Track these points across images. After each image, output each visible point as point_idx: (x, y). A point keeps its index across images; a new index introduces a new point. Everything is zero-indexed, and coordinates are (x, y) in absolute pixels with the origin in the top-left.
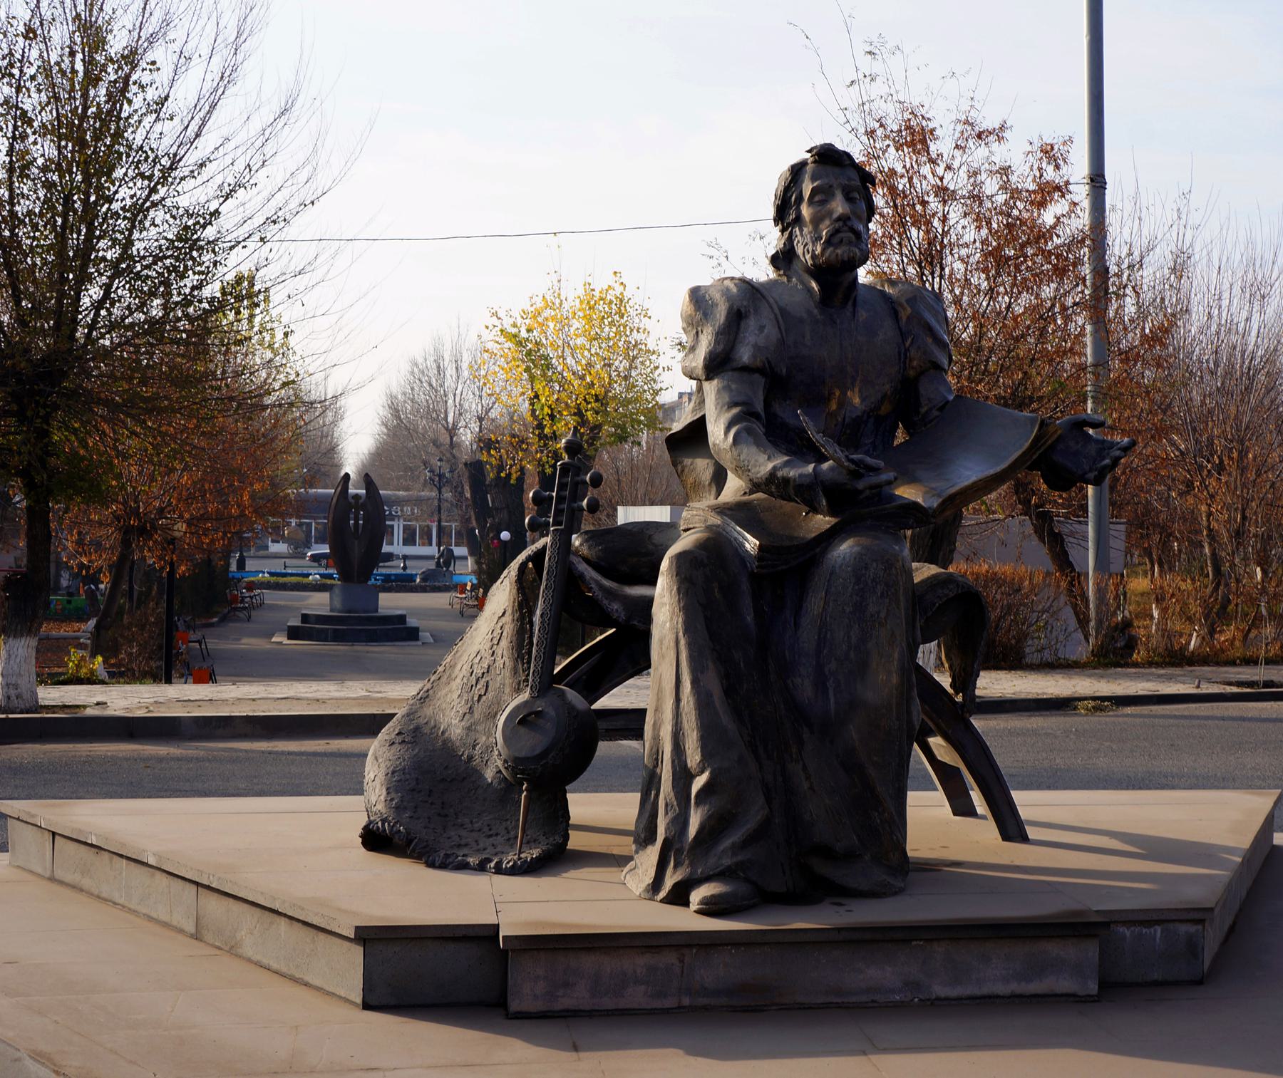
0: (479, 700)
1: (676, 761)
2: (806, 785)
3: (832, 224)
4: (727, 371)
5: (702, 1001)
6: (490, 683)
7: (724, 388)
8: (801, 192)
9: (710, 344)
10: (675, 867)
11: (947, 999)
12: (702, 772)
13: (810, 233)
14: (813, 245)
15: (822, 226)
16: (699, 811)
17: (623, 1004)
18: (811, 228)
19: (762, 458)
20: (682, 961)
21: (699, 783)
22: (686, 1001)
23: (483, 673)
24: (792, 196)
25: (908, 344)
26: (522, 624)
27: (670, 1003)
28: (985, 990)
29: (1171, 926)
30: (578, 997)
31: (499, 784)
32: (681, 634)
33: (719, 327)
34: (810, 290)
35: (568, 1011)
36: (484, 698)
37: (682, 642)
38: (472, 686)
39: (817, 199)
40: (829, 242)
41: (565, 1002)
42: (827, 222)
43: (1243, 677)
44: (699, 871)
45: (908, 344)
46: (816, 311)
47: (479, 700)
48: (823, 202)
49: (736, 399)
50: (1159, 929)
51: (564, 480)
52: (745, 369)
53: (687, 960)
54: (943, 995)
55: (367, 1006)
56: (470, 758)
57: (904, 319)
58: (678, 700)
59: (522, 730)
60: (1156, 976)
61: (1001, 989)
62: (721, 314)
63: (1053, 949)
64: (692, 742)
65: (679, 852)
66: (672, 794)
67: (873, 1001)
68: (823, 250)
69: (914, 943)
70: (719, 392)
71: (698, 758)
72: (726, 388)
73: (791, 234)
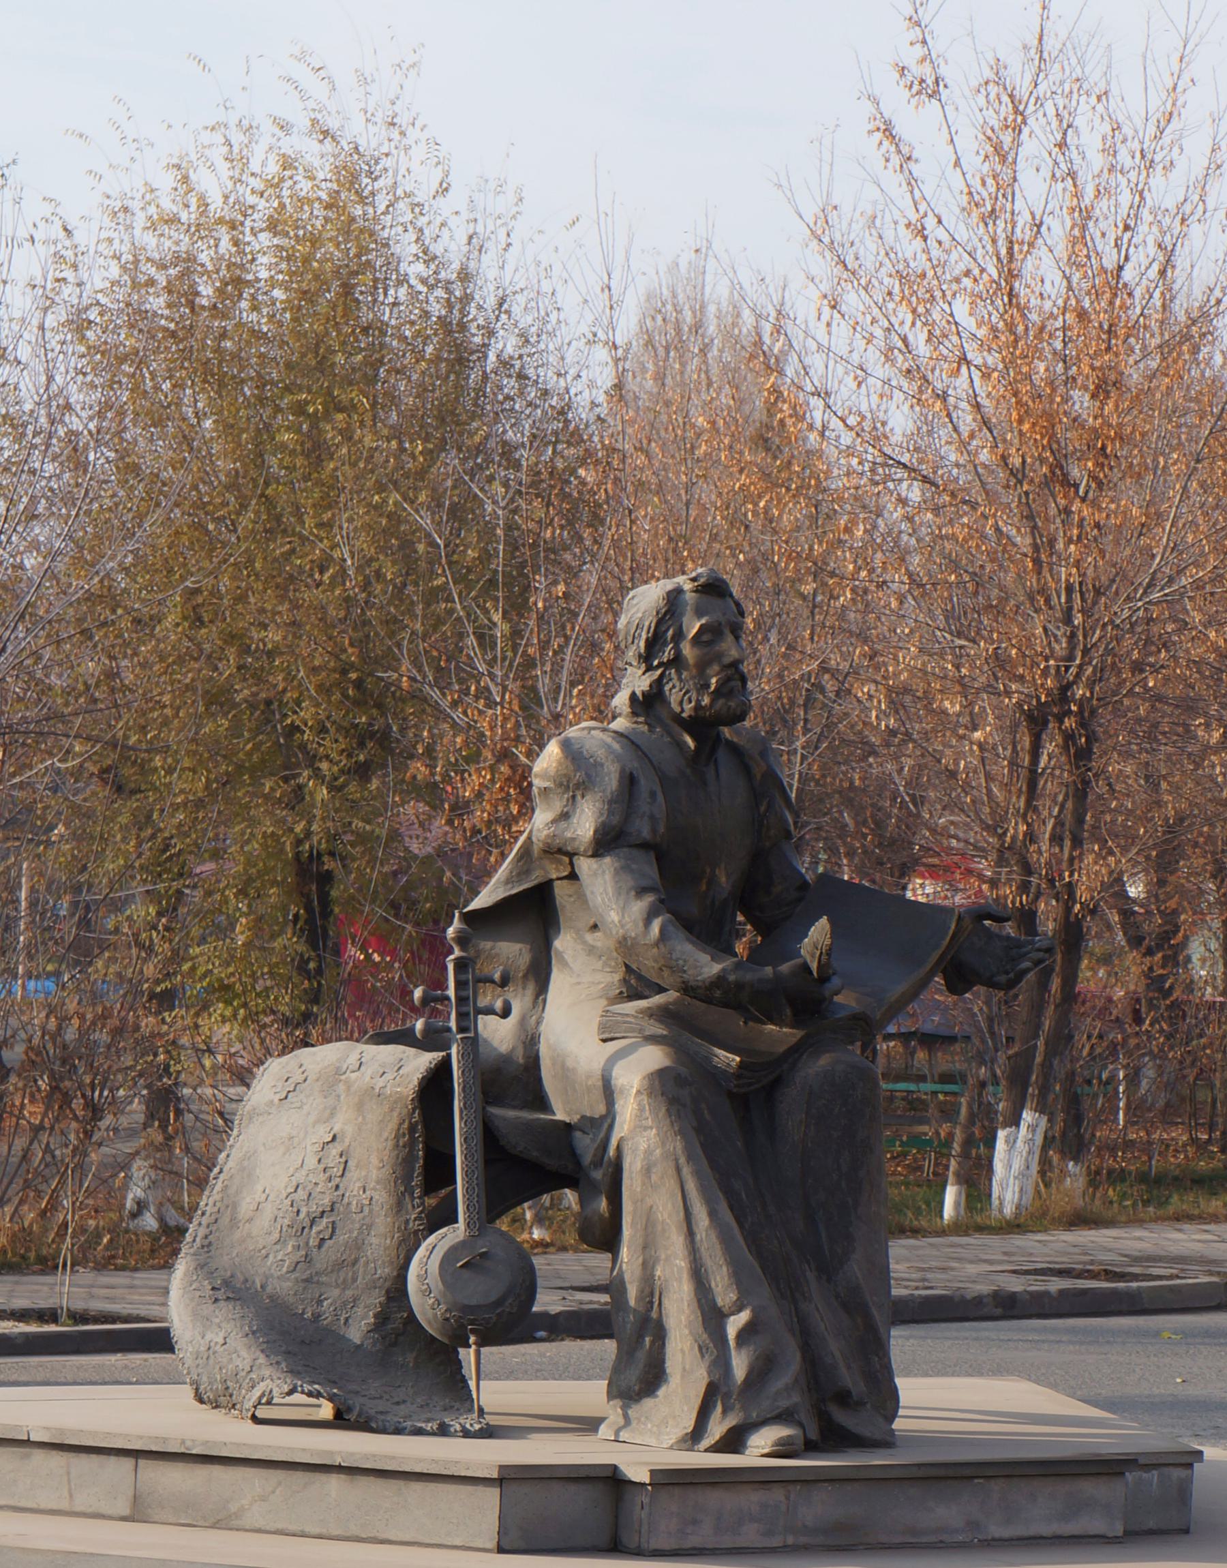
0: (320, 1246)
1: (703, 1301)
2: (822, 1327)
3: (722, 670)
4: (623, 846)
5: (803, 1540)
6: (339, 1225)
7: (622, 868)
8: (681, 627)
9: (602, 814)
10: (724, 1412)
11: (1000, 1540)
12: (740, 1310)
13: (693, 678)
14: (698, 694)
15: (709, 671)
16: (744, 1352)
17: (741, 1542)
18: (694, 671)
19: (704, 958)
20: (788, 1498)
21: (735, 1324)
22: (790, 1540)
23: (323, 1212)
24: (667, 630)
25: (762, 809)
26: (411, 1151)
27: (776, 1542)
28: (1032, 1531)
29: (1166, 1470)
30: (703, 1536)
31: (374, 1344)
32: (682, 1160)
33: (612, 793)
34: (681, 745)
35: (695, 1549)
36: (329, 1243)
37: (686, 1171)
38: (303, 1228)
39: (705, 638)
40: (717, 694)
41: (694, 1541)
42: (716, 668)
43: (20, 1303)
44: (754, 1415)
45: (762, 809)
46: (688, 771)
47: (320, 1246)
48: (709, 643)
49: (646, 883)
50: (1155, 1472)
51: (463, 977)
52: (645, 846)
53: (792, 1497)
54: (997, 1535)
55: (501, 1550)
56: (317, 1317)
57: (759, 777)
58: (690, 1234)
59: (466, 1274)
60: (1151, 1524)
61: (1046, 1530)
62: (611, 780)
63: (1090, 1488)
64: (722, 1278)
65: (727, 1396)
66: (705, 1336)
67: (941, 1542)
68: (713, 701)
69: (976, 1481)
70: (617, 872)
71: (733, 1296)
72: (626, 868)
73: (662, 676)
